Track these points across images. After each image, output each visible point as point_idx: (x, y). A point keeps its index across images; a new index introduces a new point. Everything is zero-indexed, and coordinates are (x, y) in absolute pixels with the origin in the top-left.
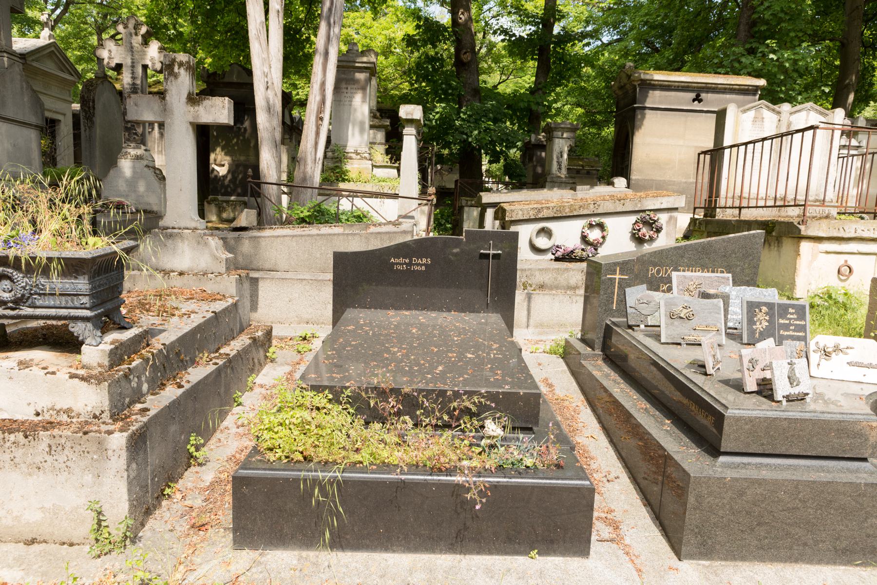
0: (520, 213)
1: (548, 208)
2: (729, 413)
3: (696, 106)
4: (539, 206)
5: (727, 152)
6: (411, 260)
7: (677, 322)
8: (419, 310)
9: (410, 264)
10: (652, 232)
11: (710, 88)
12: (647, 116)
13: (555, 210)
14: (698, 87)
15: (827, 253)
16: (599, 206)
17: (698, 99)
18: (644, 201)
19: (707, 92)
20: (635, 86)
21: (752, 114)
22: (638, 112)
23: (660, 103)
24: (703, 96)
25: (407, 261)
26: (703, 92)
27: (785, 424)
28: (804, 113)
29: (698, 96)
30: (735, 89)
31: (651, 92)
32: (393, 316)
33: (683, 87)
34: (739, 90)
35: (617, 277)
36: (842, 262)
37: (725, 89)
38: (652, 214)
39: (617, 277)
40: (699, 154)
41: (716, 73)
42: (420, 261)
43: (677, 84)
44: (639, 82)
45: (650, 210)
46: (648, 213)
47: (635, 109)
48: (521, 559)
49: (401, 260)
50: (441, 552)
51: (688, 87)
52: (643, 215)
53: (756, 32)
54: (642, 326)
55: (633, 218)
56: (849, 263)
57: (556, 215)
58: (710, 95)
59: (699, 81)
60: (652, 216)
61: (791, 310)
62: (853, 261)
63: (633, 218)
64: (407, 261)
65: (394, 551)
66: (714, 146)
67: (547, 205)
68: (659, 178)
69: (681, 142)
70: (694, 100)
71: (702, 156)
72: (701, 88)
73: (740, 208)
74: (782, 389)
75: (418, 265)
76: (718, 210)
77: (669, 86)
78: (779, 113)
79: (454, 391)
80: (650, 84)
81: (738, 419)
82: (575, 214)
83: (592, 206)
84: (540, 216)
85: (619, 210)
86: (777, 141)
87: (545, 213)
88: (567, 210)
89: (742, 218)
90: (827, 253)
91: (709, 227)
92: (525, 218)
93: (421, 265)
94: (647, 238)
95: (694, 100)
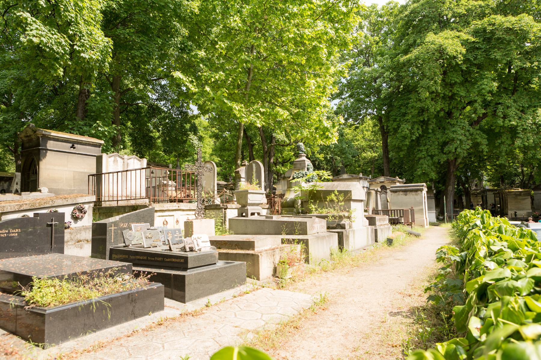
0: (9, 207)
1: (26, 204)
2: (189, 256)
3: (72, 150)
4: (21, 204)
5: (103, 175)
6: (9, 231)
7: (148, 239)
8: (14, 257)
9: (9, 233)
10: (82, 214)
11: (79, 142)
12: (48, 154)
13: (30, 205)
14: (73, 141)
15: (159, 216)
16: (54, 202)
17: (73, 147)
18: (77, 198)
19: (78, 144)
20: (39, 137)
21: (112, 158)
22: (42, 151)
23: (53, 147)
24: (76, 145)
25: (7, 231)
26: (75, 144)
27: (200, 256)
28: (132, 159)
29: (73, 145)
30: (91, 144)
31: (49, 141)
32: (12, 260)
33: (65, 140)
34: (92, 144)
35: (113, 228)
36: (164, 220)
37: (86, 143)
38: (82, 205)
39: (113, 228)
40: (89, 176)
41: (71, 133)
42: (14, 231)
43: (62, 138)
44: (42, 135)
45: (81, 203)
46: (80, 204)
47: (39, 149)
48: (147, 317)
49: (4, 231)
50: (123, 322)
51: (68, 140)
52: (78, 206)
53: (88, 115)
54: (131, 245)
55: (72, 208)
56: (166, 220)
57: (31, 208)
58: (79, 146)
59: (74, 138)
60: (82, 206)
61: (177, 231)
62: (167, 219)
63: (72, 208)
64: (7, 231)
65: (108, 328)
66: (97, 172)
67: (26, 203)
68: (55, 188)
69: (66, 169)
70: (71, 147)
71: (91, 177)
72: (74, 142)
73: (118, 201)
74: (196, 248)
75: (13, 233)
76: (103, 202)
77: (58, 139)
78: (123, 159)
79: (105, 269)
80: (48, 137)
81: (191, 257)
82: (42, 207)
83: (51, 202)
84: (22, 209)
85: (65, 203)
86: (138, 172)
87: (25, 207)
88: (37, 205)
89: (119, 205)
90: (159, 216)
91: (101, 211)
92: (12, 210)
93: (15, 233)
94: (80, 217)
95: (71, 147)
